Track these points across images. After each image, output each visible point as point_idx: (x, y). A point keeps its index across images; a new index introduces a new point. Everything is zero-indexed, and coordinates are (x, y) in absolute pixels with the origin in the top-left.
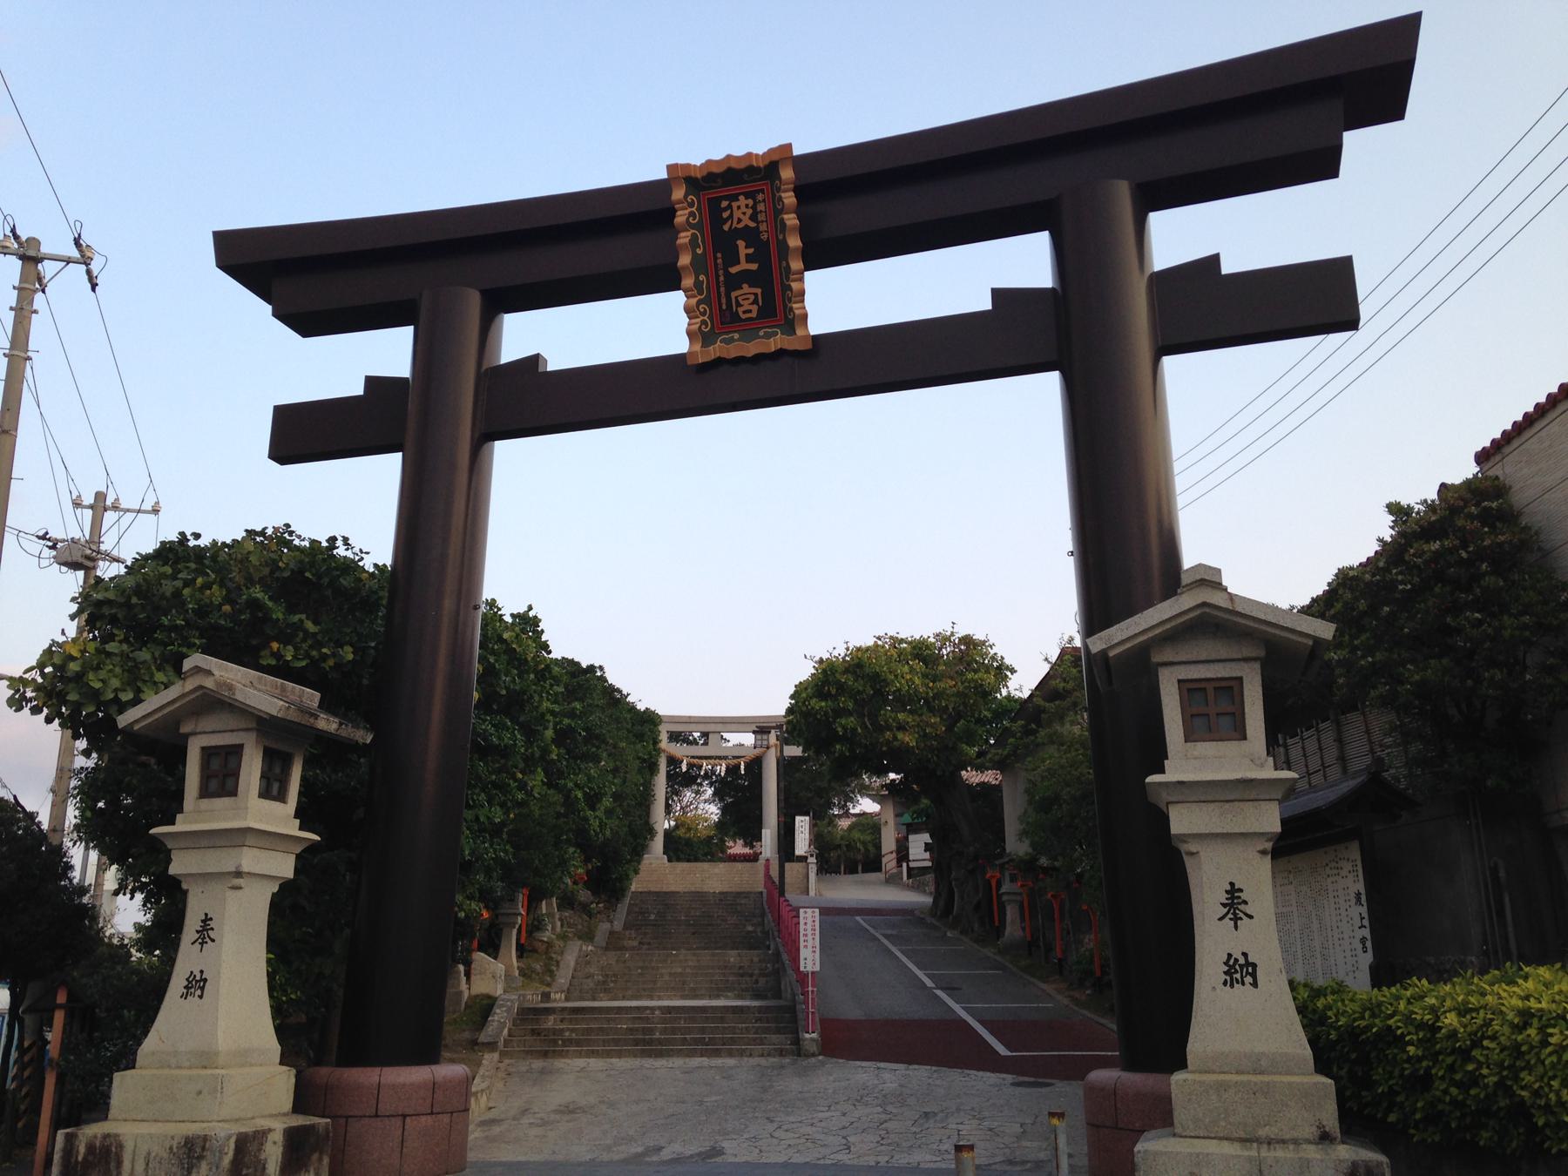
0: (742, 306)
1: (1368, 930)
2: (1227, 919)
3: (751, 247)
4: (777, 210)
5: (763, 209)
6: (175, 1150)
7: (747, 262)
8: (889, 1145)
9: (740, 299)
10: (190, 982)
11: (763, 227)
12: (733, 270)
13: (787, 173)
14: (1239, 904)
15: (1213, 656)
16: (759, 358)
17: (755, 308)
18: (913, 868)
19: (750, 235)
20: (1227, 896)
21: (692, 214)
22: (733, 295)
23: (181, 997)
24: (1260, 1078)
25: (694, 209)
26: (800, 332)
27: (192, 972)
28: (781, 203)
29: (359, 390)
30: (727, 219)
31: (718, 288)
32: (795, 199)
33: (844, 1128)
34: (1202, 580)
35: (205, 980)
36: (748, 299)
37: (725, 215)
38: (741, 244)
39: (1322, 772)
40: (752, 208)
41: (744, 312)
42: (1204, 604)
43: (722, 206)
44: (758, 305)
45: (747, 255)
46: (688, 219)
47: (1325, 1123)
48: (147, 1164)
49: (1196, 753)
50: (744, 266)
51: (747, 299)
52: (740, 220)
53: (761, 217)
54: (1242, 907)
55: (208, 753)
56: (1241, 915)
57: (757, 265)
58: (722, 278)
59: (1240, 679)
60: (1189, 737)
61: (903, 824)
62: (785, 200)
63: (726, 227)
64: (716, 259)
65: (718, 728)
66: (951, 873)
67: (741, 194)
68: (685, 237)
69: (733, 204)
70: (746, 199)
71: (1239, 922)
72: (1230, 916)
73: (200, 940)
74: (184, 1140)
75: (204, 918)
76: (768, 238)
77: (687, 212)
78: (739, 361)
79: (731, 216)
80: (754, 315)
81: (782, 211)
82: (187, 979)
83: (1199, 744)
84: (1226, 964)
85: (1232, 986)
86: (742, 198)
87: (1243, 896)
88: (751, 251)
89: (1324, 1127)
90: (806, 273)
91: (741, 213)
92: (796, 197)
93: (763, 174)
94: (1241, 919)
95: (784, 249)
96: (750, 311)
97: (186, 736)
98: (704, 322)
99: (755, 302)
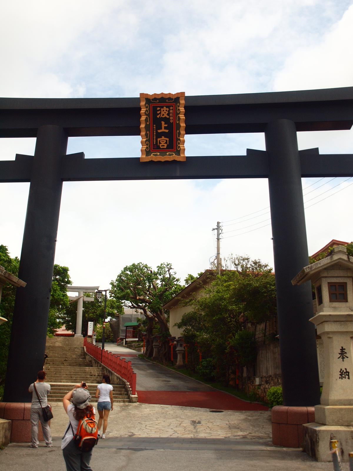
0: (161, 144)
3: (167, 124)
4: (177, 113)
5: (172, 112)
7: (164, 129)
9: (161, 141)
11: (171, 118)
12: (159, 131)
13: (182, 102)
14: (344, 353)
15: (339, 275)
16: (167, 162)
17: (166, 145)
19: (167, 120)
20: (341, 351)
21: (146, 111)
25: (148, 109)
26: (182, 155)
28: (179, 111)
29: (14, 159)
31: (153, 136)
32: (184, 110)
33: (169, 426)
34: (340, 251)
36: (164, 141)
37: (158, 112)
38: (163, 123)
40: (168, 111)
41: (162, 146)
42: (340, 259)
44: (167, 144)
45: (165, 127)
46: (145, 112)
49: (333, 306)
50: (163, 130)
51: (163, 142)
52: (163, 115)
53: (171, 115)
54: (345, 354)
56: (345, 357)
57: (168, 130)
58: (155, 133)
59: (346, 283)
60: (331, 300)
61: (125, 326)
62: (181, 110)
63: (158, 116)
67: (165, 106)
68: (144, 118)
69: (161, 109)
70: (166, 108)
71: (344, 359)
72: (341, 357)
75: (341, 348)
76: (173, 122)
77: (145, 109)
78: (159, 162)
79: (160, 113)
81: (179, 114)
84: (340, 372)
85: (342, 379)
86: (165, 107)
87: (345, 351)
88: (166, 125)
90: (185, 135)
91: (164, 112)
93: (173, 101)
94: (344, 358)
95: (179, 126)
96: (164, 146)
98: (147, 148)
99: (166, 143)
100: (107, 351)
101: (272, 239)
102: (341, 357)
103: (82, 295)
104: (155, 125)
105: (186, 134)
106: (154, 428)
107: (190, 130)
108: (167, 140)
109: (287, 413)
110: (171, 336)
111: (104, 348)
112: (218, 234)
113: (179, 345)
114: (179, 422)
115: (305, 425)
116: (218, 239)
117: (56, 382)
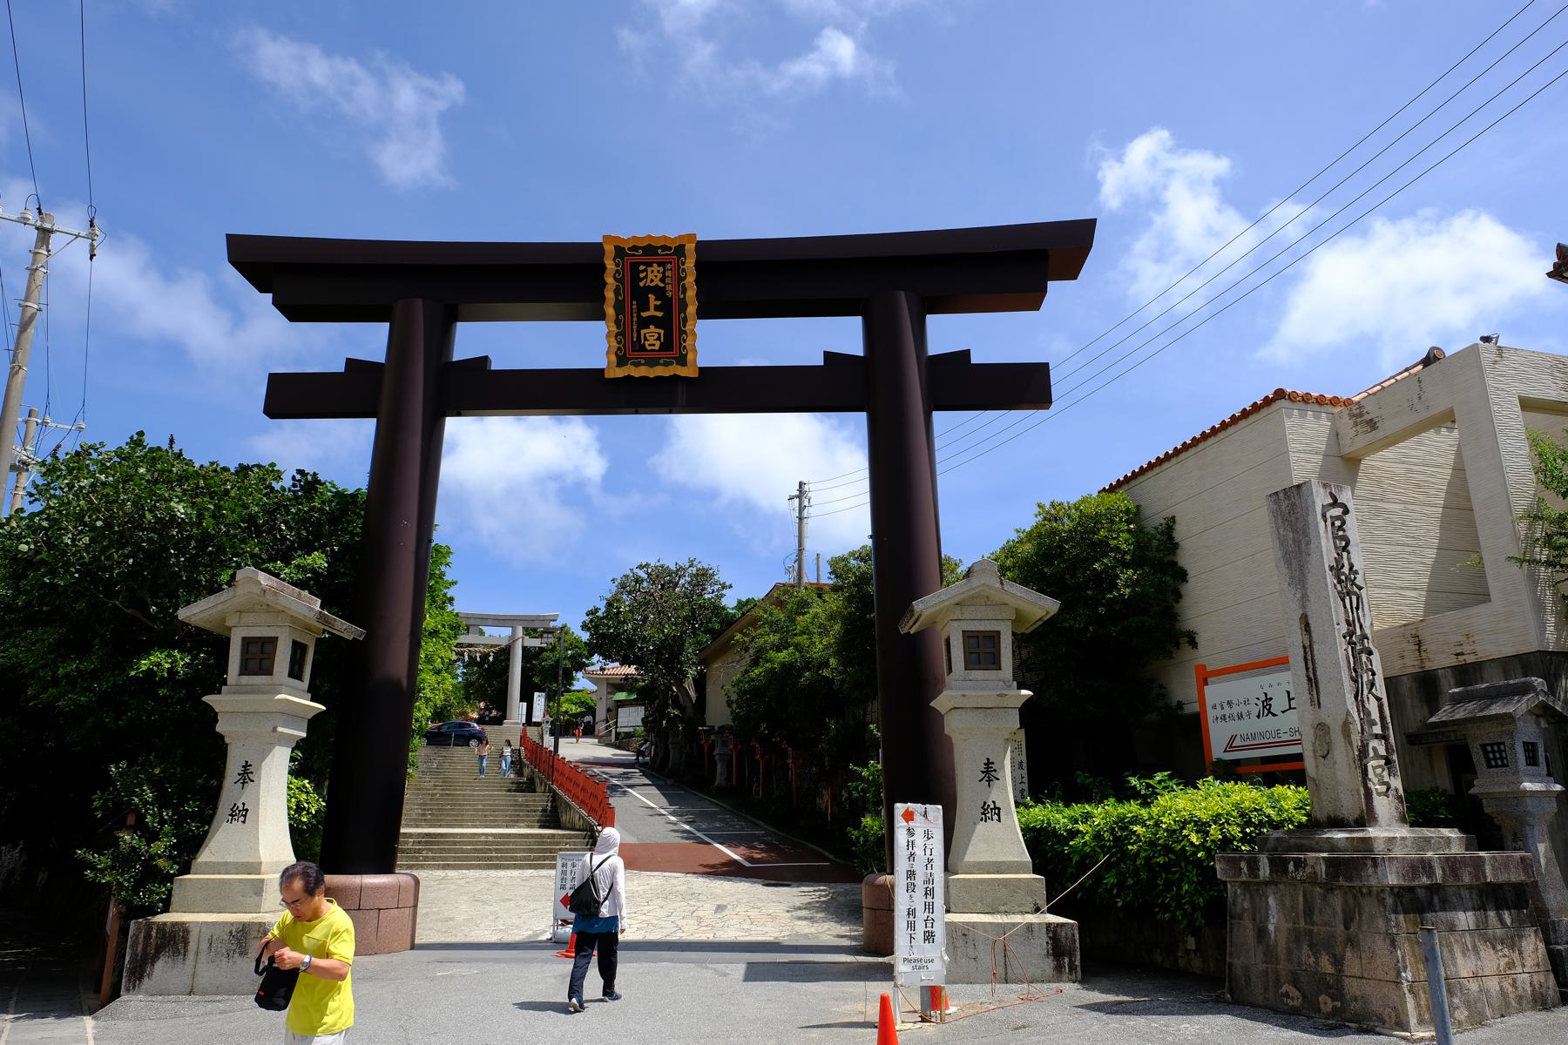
1: (1027, 785)
6: (234, 933)
8: (707, 926)
11: (669, 288)
12: (644, 314)
18: (620, 733)
19: (659, 292)
22: (643, 332)
25: (619, 268)
27: (235, 804)
31: (632, 325)
33: (668, 916)
37: (642, 275)
38: (652, 297)
41: (650, 345)
45: (655, 305)
50: (652, 312)
52: (652, 281)
55: (247, 642)
58: (635, 319)
59: (999, 632)
64: (632, 305)
65: (478, 622)
72: (986, 779)
73: (242, 781)
79: (646, 277)
80: (657, 348)
82: (232, 809)
84: (983, 808)
86: (655, 265)
88: (659, 303)
91: (653, 276)
96: (654, 345)
97: (229, 629)
99: (659, 339)
101: (871, 537)
102: (986, 779)
103: (521, 635)
104: (634, 302)
107: (703, 314)
108: (659, 334)
112: (801, 509)
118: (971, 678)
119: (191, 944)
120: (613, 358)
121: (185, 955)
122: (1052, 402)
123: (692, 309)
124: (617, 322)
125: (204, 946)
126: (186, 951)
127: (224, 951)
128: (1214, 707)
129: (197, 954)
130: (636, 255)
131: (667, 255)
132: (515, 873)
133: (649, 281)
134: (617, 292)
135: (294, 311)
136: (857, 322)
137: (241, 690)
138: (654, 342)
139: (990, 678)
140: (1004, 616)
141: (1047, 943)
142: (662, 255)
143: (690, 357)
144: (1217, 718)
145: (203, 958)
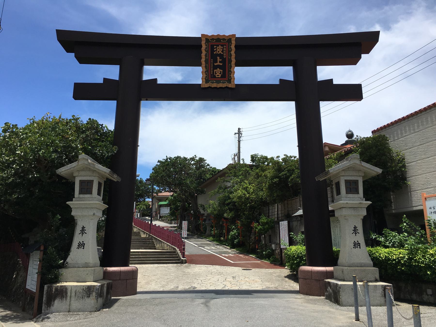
2: (354, 234)
6: (84, 289)
7: (219, 63)
9: (216, 72)
10: (79, 244)
11: (225, 54)
12: (215, 64)
13: (233, 42)
14: (356, 230)
17: (220, 75)
19: (221, 56)
21: (206, 48)
22: (215, 71)
23: (77, 248)
24: (362, 268)
27: (80, 242)
28: (231, 49)
30: (215, 51)
31: (211, 68)
35: (84, 244)
37: (215, 50)
38: (218, 58)
39: (299, 198)
41: (217, 76)
42: (355, 163)
43: (214, 47)
45: (220, 61)
47: (376, 277)
48: (76, 294)
50: (218, 63)
51: (218, 72)
52: (219, 52)
53: (224, 52)
54: (357, 231)
55: (81, 182)
57: (222, 64)
58: (212, 66)
59: (358, 181)
60: (347, 193)
64: (211, 60)
66: (185, 218)
69: (217, 47)
70: (221, 46)
73: (82, 233)
74: (87, 287)
76: (226, 57)
79: (216, 50)
80: (220, 77)
82: (78, 244)
83: (349, 194)
86: (220, 46)
88: (221, 60)
89: (376, 278)
91: (219, 50)
92: (235, 48)
96: (219, 76)
97: (74, 177)
99: (220, 73)
100: (155, 225)
101: (138, 146)
104: (212, 60)
105: (236, 66)
106: (208, 282)
109: (311, 272)
110: (201, 212)
111: (152, 222)
112: (239, 137)
113: (208, 220)
114: (225, 278)
115: (327, 280)
116: (239, 141)
117: (151, 252)
118: (348, 197)
119: (68, 293)
120: (204, 80)
121: (66, 297)
122: (362, 98)
123: (233, 62)
124: (206, 67)
125: (73, 294)
126: (66, 296)
127: (81, 296)
128: (431, 208)
129: (71, 297)
130: (213, 42)
131: (224, 42)
132: (152, 265)
133: (217, 52)
134: (206, 55)
135: (82, 60)
136: (291, 68)
137: (80, 199)
138: (219, 75)
139: (355, 197)
140: (360, 174)
141: (382, 292)
142: (223, 42)
143: (232, 80)
144: (432, 213)
145: (73, 299)
